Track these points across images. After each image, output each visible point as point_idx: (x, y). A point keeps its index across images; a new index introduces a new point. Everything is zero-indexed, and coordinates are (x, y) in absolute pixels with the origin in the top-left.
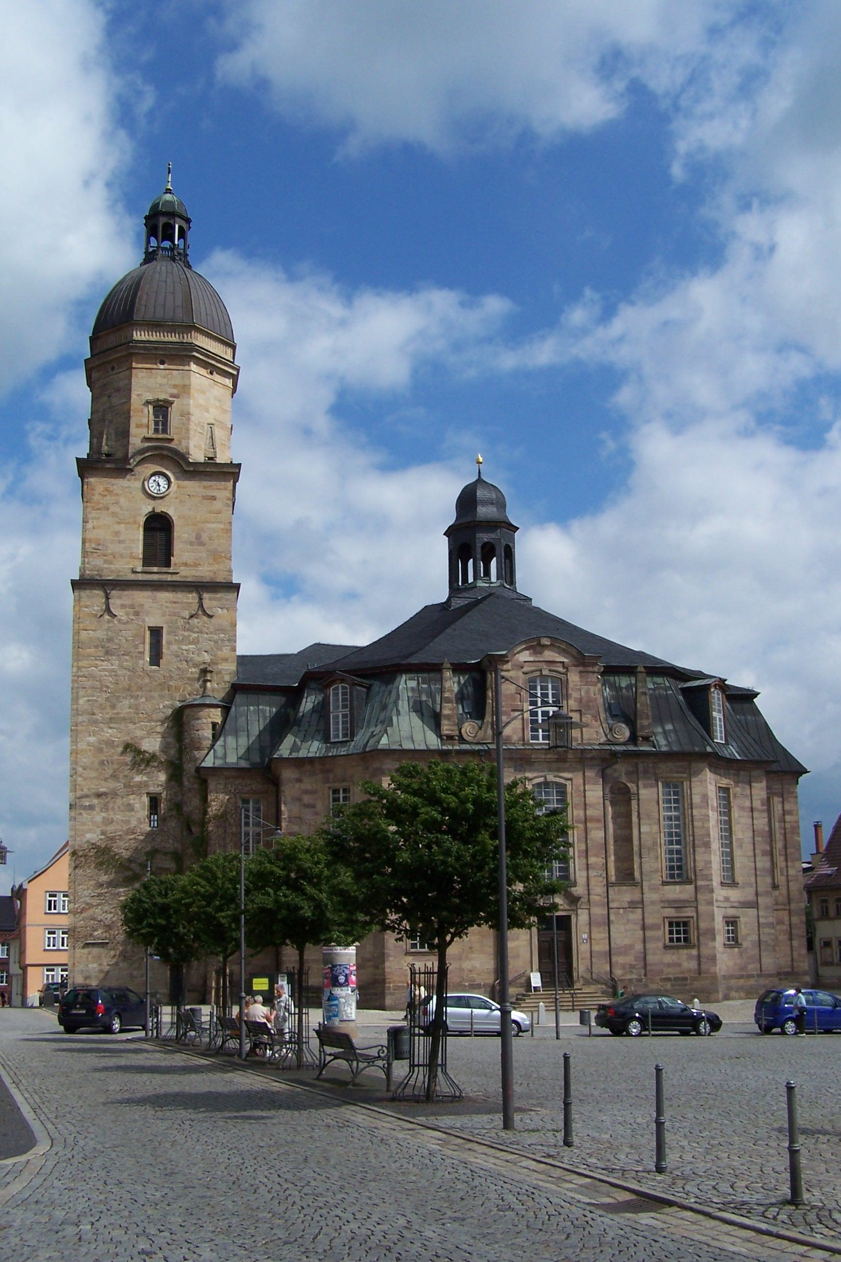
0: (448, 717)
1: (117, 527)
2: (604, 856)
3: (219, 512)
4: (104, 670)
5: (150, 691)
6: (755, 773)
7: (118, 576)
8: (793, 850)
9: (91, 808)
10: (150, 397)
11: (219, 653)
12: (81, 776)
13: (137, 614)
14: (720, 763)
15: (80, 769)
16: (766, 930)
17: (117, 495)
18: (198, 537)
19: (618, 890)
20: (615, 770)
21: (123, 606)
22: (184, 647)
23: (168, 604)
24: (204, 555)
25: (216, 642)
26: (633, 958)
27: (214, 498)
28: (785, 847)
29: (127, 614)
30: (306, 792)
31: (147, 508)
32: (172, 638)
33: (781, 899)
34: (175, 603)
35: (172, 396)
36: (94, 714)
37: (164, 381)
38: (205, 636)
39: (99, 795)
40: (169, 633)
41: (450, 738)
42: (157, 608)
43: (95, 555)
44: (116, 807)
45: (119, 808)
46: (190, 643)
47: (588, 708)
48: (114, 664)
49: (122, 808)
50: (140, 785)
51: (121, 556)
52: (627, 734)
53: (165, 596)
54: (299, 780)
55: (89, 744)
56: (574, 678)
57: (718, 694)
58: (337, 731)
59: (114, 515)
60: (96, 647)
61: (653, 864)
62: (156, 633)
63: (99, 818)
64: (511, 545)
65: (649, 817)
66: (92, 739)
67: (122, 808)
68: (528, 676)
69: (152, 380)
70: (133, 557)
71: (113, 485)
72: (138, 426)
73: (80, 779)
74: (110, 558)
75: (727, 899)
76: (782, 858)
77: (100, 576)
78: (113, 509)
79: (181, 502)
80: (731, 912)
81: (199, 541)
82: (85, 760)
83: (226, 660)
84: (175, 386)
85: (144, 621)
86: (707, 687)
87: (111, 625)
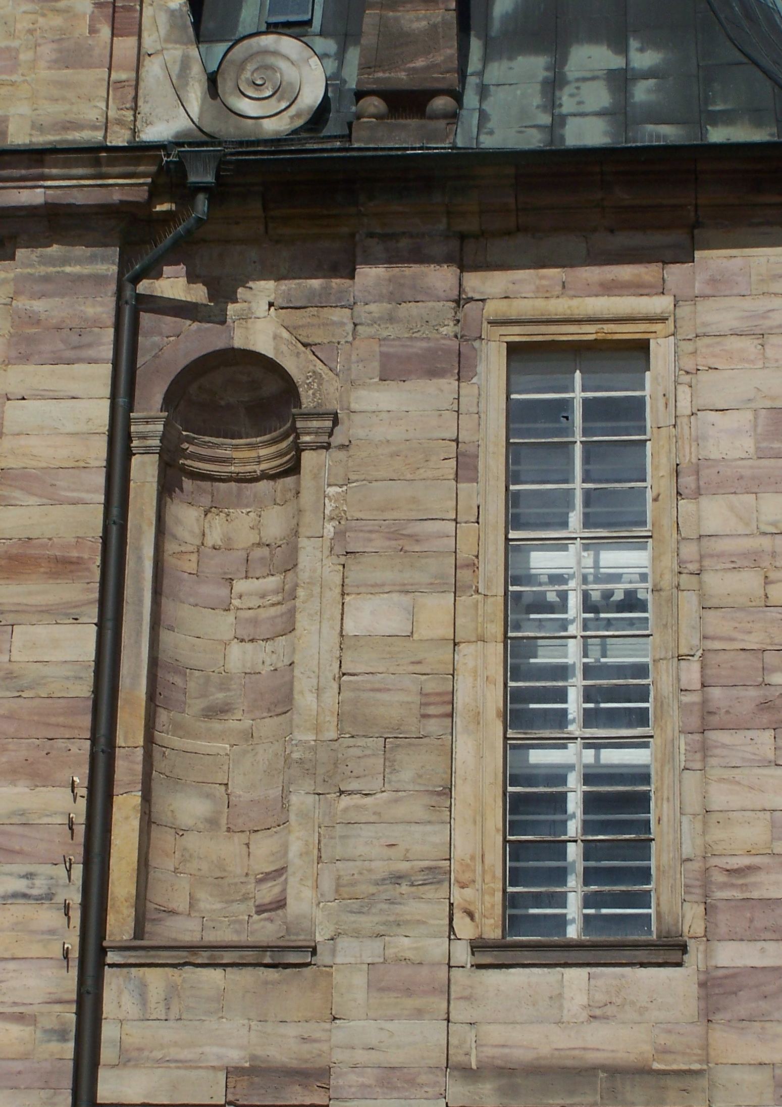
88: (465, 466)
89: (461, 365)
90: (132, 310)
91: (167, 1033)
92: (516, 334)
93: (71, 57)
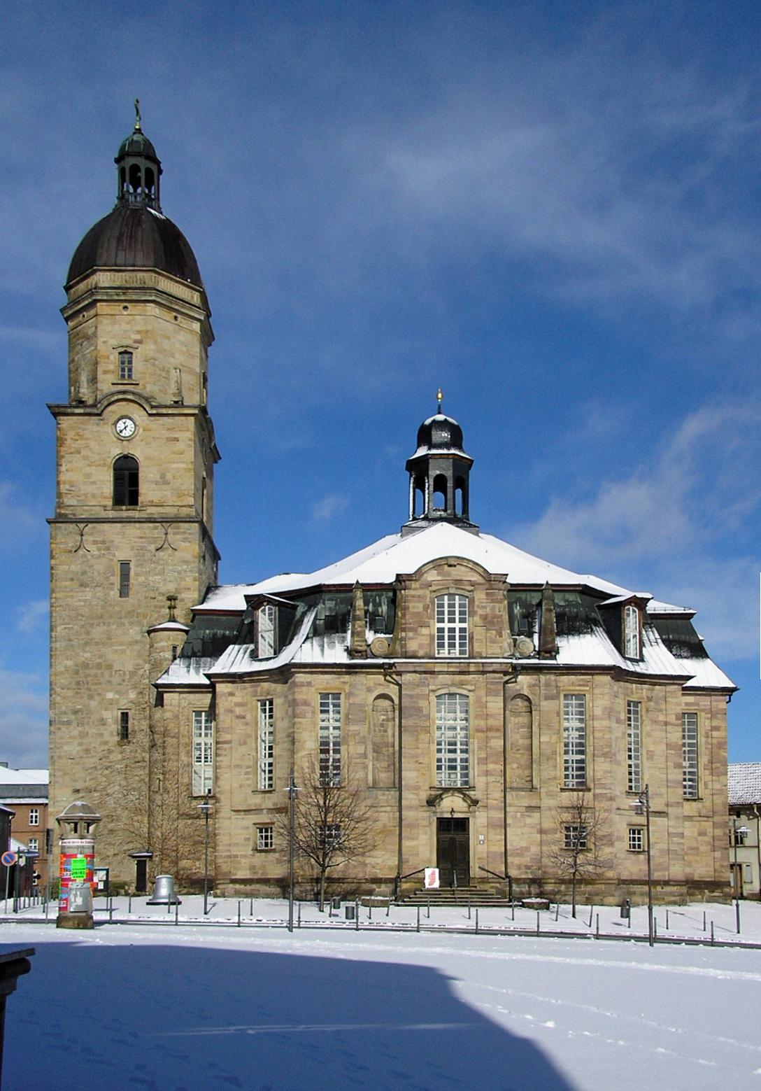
1: (88, 470)
2: (502, 763)
4: (80, 600)
5: (121, 618)
7: (91, 514)
8: (719, 765)
9: (69, 723)
10: (114, 342)
11: (183, 583)
12: (59, 695)
13: (108, 549)
15: (58, 690)
16: (675, 839)
17: (87, 439)
18: (163, 476)
19: (517, 795)
21: (95, 542)
22: (150, 578)
23: (136, 540)
24: (168, 493)
25: (179, 573)
26: (528, 859)
29: (99, 550)
30: (238, 704)
31: (116, 451)
32: (139, 569)
34: (142, 538)
35: (136, 342)
36: (71, 640)
37: (128, 327)
38: (170, 568)
42: (125, 540)
43: (69, 496)
44: (91, 723)
45: (93, 723)
46: (156, 575)
47: (492, 623)
48: (88, 594)
49: (96, 723)
50: (111, 702)
53: (133, 530)
54: (231, 694)
57: (634, 611)
58: (265, 649)
59: (85, 458)
60: (72, 580)
61: (553, 773)
63: (76, 733)
64: (464, 476)
65: (549, 727)
66: (69, 663)
67: (96, 723)
68: (435, 595)
69: (117, 326)
71: (84, 430)
72: (106, 372)
73: (59, 698)
74: (83, 498)
76: (707, 772)
77: (74, 515)
79: (147, 444)
84: (139, 332)
85: (114, 555)
87: (85, 560)
91: (516, 802)
92: (243, 720)
93: (493, 642)
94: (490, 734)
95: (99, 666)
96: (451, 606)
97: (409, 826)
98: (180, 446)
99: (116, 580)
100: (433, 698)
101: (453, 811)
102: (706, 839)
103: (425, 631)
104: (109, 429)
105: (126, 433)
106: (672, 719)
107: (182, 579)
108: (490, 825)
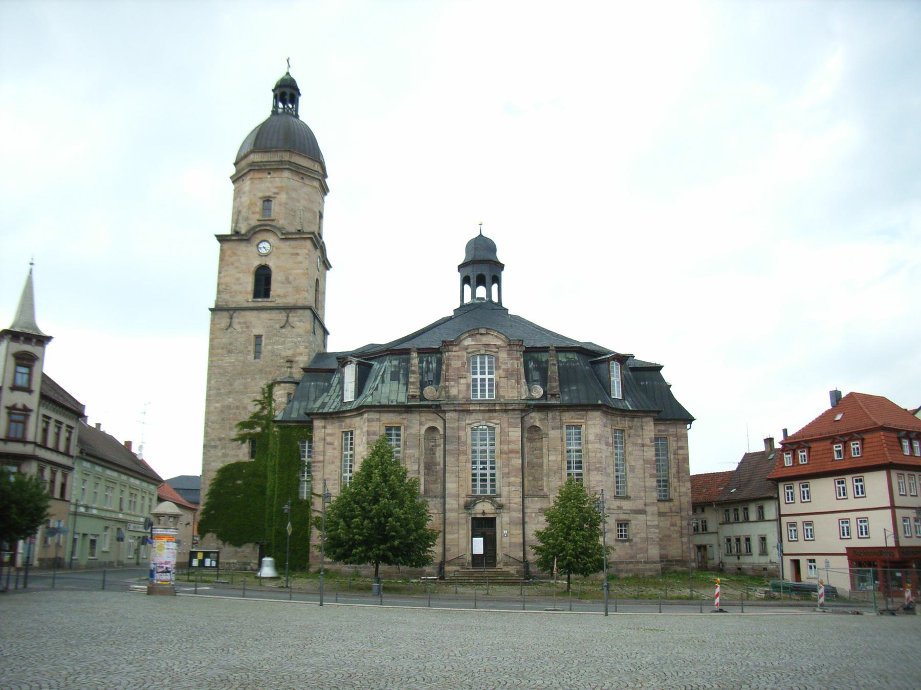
0: (413, 383)
1: (238, 275)
3: (301, 263)
6: (645, 420)
9: (215, 447)
10: (261, 195)
14: (610, 410)
18: (287, 279)
20: (531, 418)
21: (240, 323)
27: (297, 254)
28: (678, 472)
31: (257, 263)
32: (268, 341)
33: (674, 509)
39: (220, 439)
40: (266, 339)
41: (413, 397)
47: (512, 375)
48: (232, 359)
51: (241, 293)
52: (542, 393)
53: (265, 315)
55: (216, 408)
56: (503, 355)
59: (237, 267)
60: (223, 348)
62: (258, 337)
63: (220, 454)
66: (218, 405)
70: (247, 293)
75: (620, 508)
78: (236, 264)
80: (624, 517)
81: (287, 281)
82: (213, 418)
83: (301, 354)
86: (608, 360)
88: (562, 440)
89: (561, 428)
90: (522, 418)
93: (513, 388)
94: (511, 455)
95: (237, 407)
96: (482, 363)
97: (452, 524)
98: (300, 258)
99: (251, 348)
100: (469, 430)
101: (484, 513)
102: (676, 528)
103: (462, 381)
104: (254, 249)
105: (263, 251)
106: (647, 441)
107: (297, 347)
108: (511, 523)
